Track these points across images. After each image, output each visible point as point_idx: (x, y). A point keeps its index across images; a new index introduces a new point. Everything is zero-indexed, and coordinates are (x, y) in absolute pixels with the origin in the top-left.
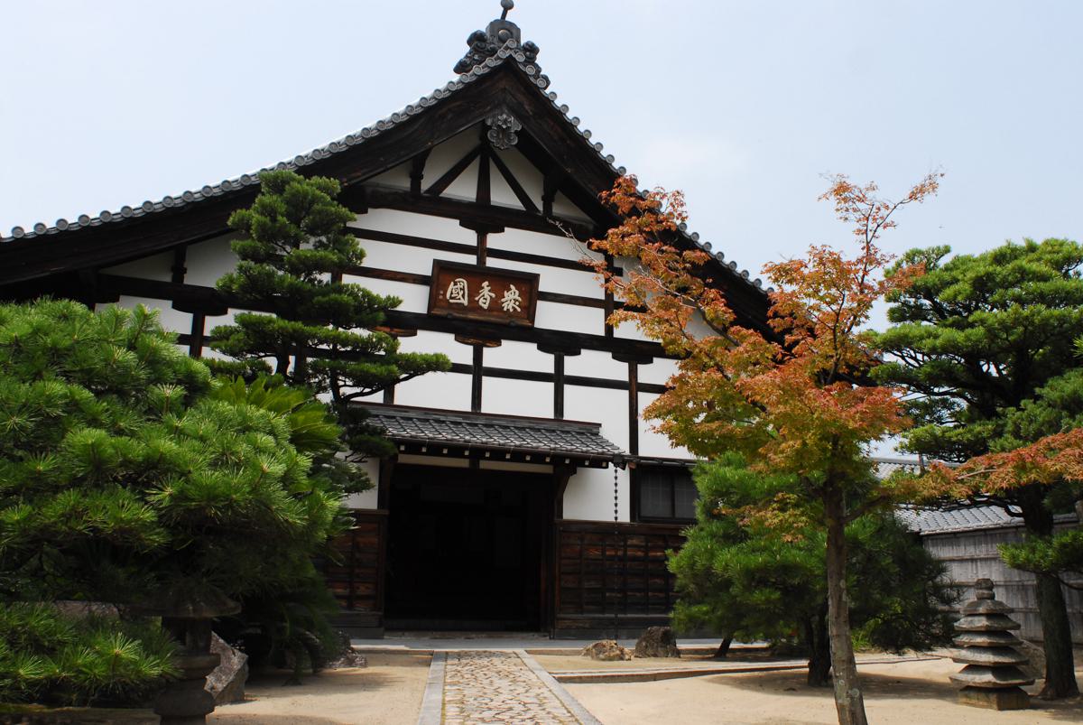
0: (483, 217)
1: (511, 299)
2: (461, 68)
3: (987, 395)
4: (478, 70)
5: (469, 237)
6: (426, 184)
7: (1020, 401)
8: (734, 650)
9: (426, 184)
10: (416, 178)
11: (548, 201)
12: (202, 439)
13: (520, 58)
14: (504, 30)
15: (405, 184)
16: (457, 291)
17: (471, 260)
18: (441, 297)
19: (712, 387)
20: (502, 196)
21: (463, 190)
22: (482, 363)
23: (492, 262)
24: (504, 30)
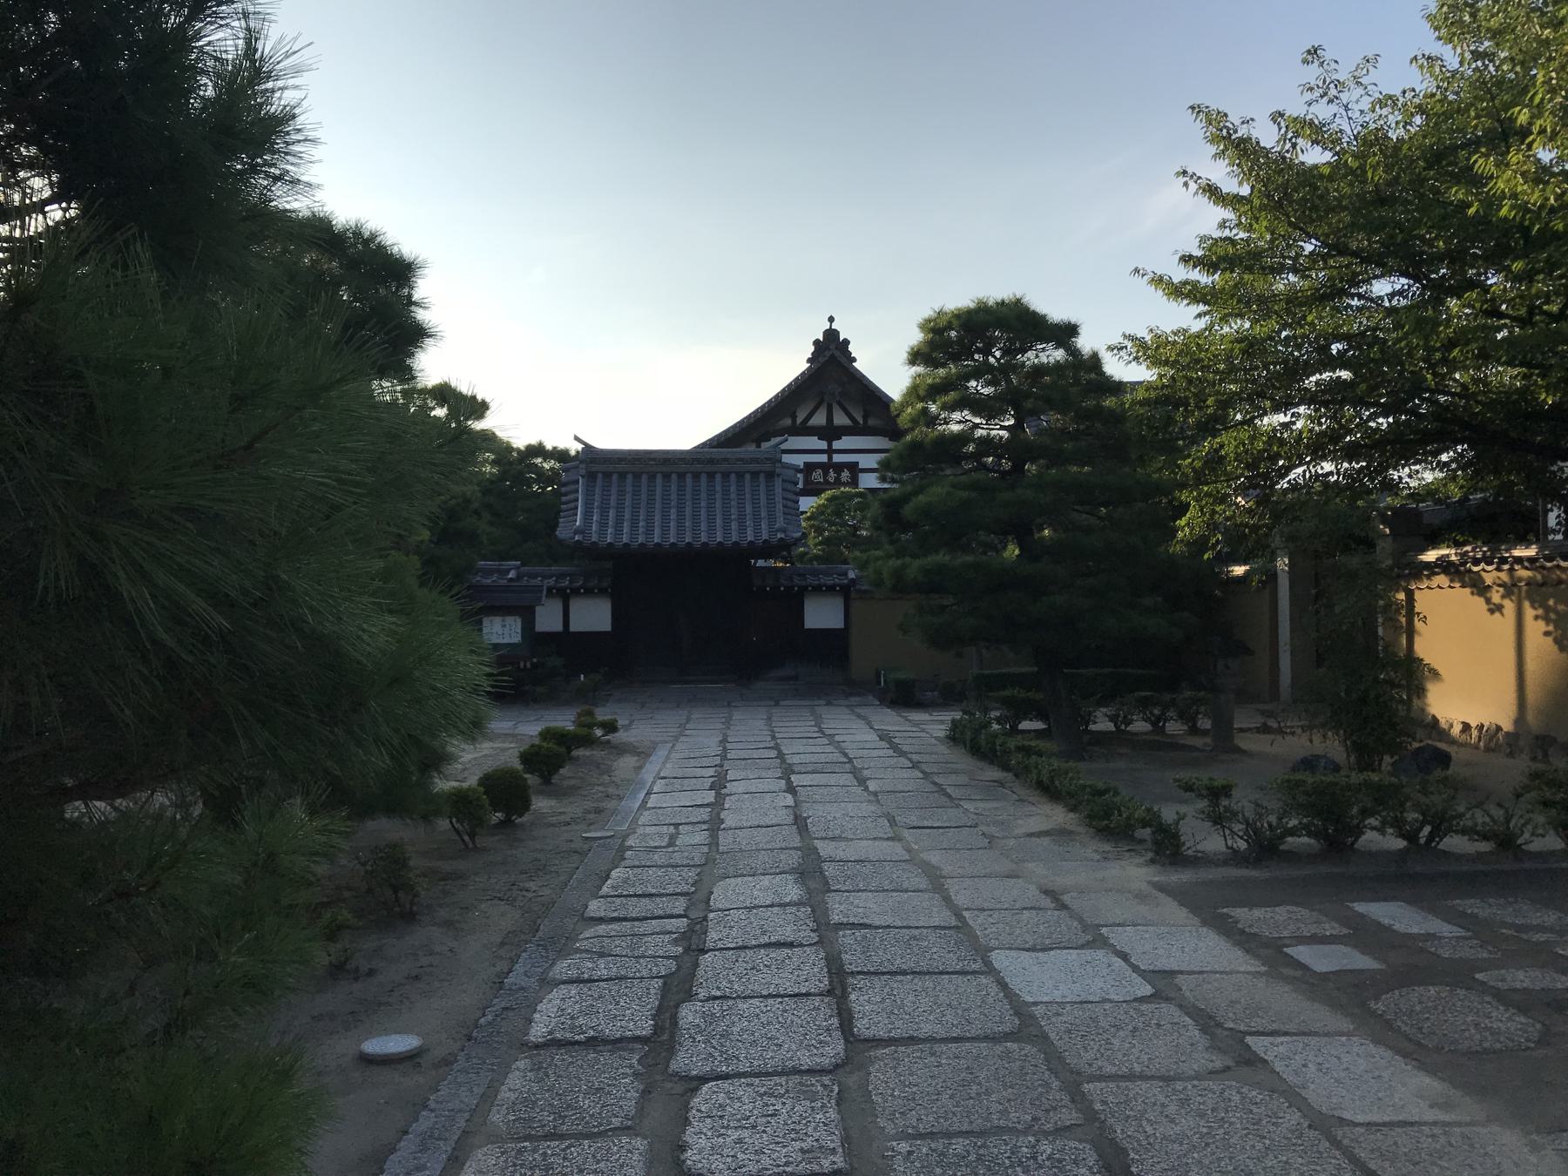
0: (830, 433)
1: (845, 475)
2: (809, 360)
3: (1471, 372)
4: (822, 360)
5: (823, 445)
6: (799, 421)
7: (79, 799)
8: (1023, 732)
9: (799, 421)
10: (794, 417)
11: (865, 417)
12: (246, 1074)
13: (837, 353)
14: (831, 334)
15: (788, 422)
16: (817, 476)
17: (823, 458)
18: (1433, 844)
19: (1526, 401)
20: (840, 419)
21: (819, 419)
22: (606, 633)
23: (837, 458)
24: (831, 334)
